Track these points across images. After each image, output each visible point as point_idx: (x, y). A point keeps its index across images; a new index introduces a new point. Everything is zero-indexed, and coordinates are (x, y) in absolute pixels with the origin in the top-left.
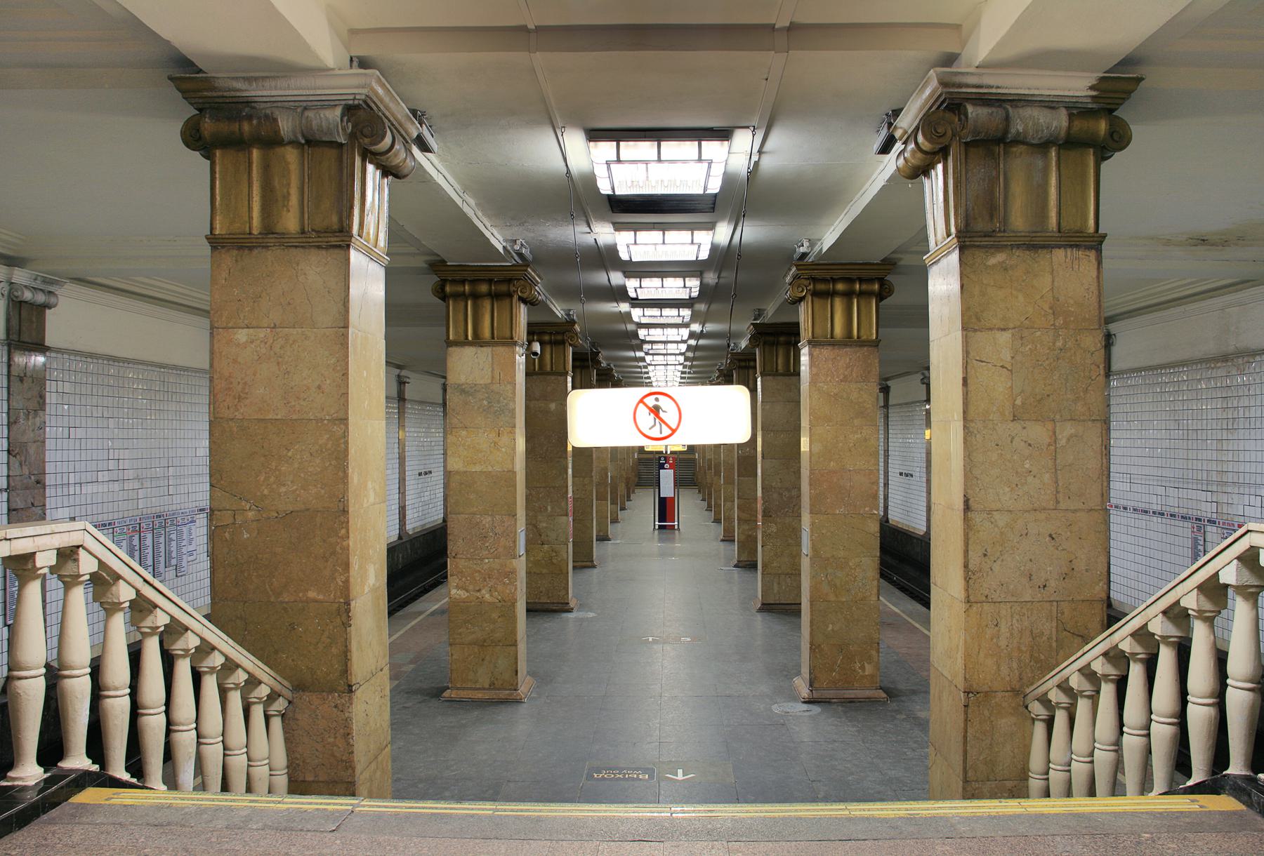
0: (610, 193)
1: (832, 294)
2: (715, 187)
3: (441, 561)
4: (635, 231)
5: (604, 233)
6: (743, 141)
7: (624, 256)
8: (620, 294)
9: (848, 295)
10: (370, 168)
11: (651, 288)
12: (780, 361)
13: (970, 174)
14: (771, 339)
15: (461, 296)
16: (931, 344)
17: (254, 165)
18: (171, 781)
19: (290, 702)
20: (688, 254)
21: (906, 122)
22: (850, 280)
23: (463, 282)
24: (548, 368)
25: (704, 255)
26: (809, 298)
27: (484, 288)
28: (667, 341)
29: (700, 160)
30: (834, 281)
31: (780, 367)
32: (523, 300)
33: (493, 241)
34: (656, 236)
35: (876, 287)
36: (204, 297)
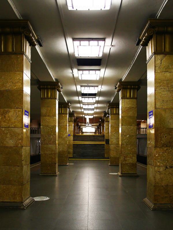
0: (81, 79)
2: (98, 79)
5: (80, 98)
6: (108, 41)
7: (83, 102)
9: (130, 89)
10: (58, 92)
11: (85, 100)
12: (115, 110)
14: (112, 106)
15: (44, 89)
19: (116, 152)
24: (63, 112)
25: (95, 102)
26: (154, 36)
27: (49, 87)
28: (88, 121)
29: (98, 45)
31: (115, 113)
32: (68, 108)
33: (65, 99)
34: (87, 99)
35: (137, 87)
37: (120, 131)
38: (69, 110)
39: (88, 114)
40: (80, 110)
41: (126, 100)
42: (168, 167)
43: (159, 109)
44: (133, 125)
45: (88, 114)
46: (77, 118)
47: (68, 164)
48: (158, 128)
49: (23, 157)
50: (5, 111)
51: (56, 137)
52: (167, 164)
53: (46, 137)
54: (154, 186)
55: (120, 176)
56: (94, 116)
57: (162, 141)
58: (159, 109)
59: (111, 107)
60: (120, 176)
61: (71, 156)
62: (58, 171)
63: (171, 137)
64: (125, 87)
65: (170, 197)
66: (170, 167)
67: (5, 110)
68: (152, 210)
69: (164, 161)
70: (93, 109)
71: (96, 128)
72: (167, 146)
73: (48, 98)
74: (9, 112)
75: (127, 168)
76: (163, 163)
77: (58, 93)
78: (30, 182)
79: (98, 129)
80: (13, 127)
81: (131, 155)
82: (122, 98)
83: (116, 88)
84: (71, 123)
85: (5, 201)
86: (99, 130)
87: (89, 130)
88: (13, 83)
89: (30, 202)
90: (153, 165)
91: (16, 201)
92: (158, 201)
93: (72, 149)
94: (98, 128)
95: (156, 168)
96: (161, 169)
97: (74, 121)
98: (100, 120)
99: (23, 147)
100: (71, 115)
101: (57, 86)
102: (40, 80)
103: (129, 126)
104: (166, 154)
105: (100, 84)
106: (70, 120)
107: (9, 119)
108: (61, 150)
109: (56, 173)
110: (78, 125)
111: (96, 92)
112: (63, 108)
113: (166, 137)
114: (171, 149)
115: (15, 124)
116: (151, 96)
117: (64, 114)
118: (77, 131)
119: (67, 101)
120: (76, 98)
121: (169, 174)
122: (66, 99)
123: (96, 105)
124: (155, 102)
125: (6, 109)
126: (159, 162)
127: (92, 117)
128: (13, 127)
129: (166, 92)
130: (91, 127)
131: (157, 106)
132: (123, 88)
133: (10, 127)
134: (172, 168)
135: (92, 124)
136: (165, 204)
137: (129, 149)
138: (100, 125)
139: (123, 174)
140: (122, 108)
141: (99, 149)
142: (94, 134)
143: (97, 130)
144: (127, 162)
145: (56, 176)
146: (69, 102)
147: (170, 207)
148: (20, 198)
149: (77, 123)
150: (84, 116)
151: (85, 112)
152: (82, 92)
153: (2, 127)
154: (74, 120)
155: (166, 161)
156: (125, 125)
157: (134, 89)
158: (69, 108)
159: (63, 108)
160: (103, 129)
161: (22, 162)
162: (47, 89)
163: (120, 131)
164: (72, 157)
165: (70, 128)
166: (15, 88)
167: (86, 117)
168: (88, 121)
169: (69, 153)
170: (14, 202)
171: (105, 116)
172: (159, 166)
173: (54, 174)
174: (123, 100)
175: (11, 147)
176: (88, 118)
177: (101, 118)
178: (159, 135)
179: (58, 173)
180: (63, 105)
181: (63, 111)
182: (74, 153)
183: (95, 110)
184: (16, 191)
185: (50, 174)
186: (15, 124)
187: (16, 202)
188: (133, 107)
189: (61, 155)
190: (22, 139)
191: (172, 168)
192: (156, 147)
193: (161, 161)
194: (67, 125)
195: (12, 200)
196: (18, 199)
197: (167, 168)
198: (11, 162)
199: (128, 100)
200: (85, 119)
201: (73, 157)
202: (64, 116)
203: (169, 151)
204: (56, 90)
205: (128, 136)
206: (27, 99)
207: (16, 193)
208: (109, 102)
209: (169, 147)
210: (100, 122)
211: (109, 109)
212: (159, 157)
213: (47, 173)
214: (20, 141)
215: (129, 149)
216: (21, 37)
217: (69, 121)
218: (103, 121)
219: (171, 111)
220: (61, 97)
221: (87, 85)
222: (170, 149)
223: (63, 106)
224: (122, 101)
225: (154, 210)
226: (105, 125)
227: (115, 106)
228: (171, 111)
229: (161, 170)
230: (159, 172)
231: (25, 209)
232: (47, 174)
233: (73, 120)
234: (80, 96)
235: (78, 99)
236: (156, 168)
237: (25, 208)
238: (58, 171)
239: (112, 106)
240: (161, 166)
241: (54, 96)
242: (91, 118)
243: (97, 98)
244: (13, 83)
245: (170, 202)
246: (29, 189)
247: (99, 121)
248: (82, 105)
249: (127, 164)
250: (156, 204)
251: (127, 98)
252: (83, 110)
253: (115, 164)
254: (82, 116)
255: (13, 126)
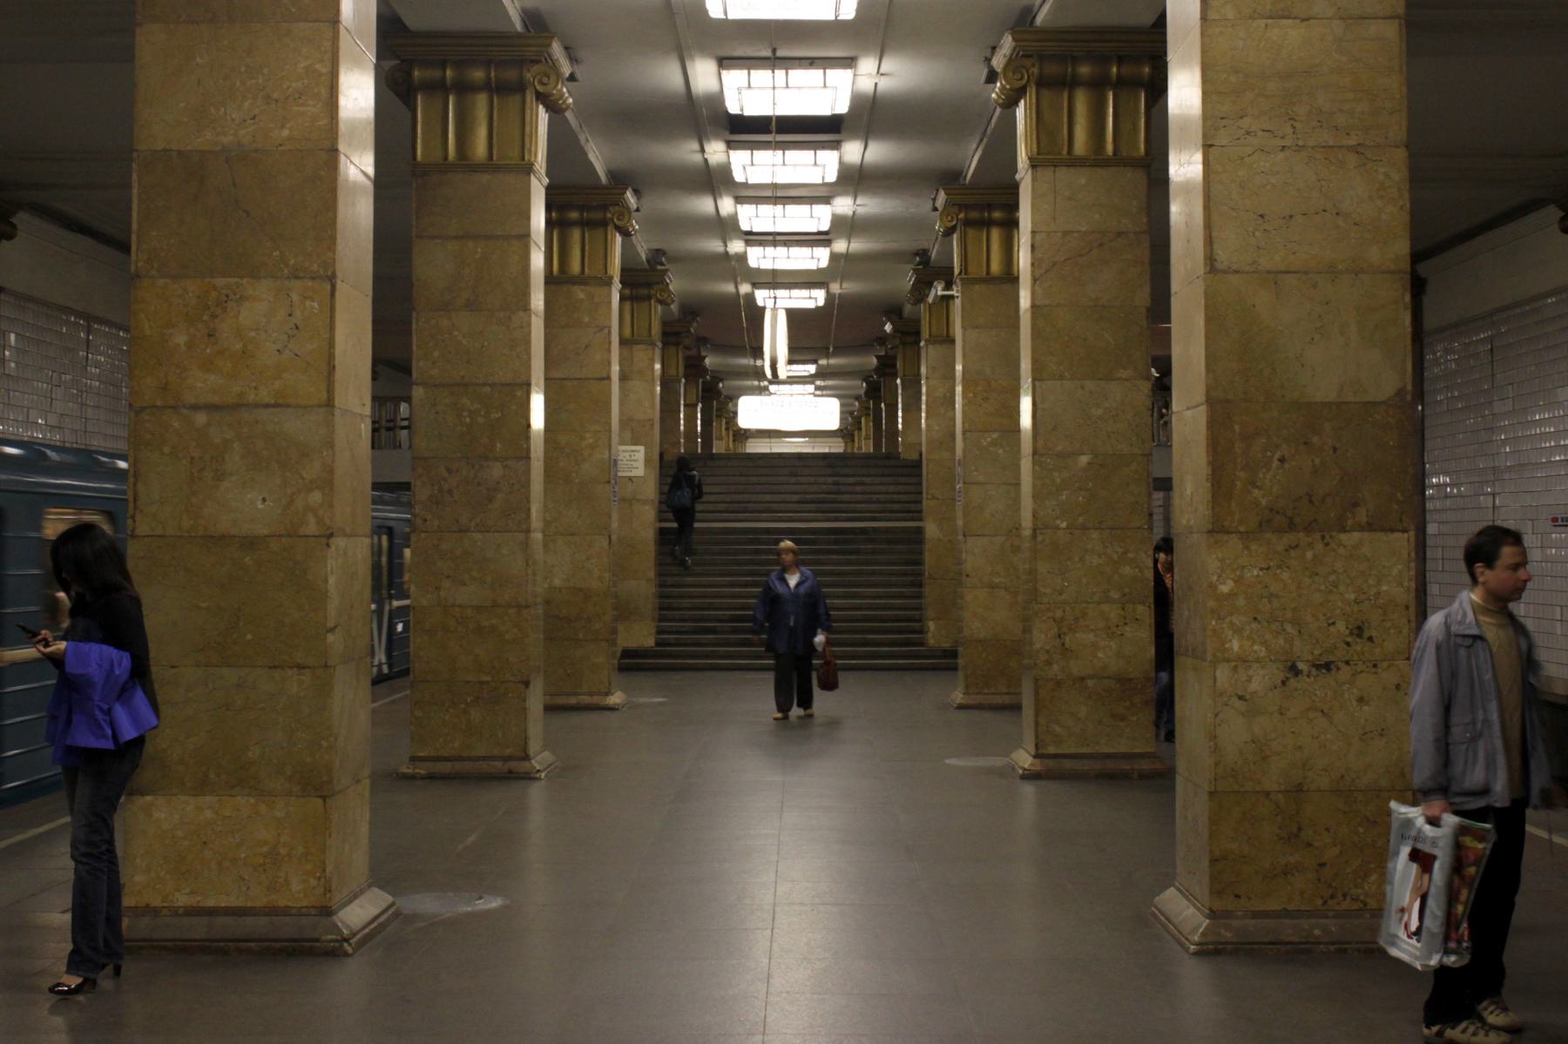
0: (722, 16)
1: (1071, 84)
3: (1395, 825)
4: (815, 150)
5: (716, 151)
6: (867, 65)
7: (739, 176)
8: (727, 227)
9: (1098, 85)
10: (541, 109)
11: (754, 165)
13: (355, 929)
14: (974, 215)
15: (437, 88)
16: (1173, 299)
17: (419, 141)
18: (124, 492)
20: (812, 176)
21: (998, 62)
22: (1103, 60)
23: (443, 65)
25: (832, 177)
26: (1031, 92)
28: (776, 337)
30: (1075, 60)
32: (542, 98)
33: (592, 157)
36: (33, 609)
37: (1026, 420)
38: (628, 249)
39: (776, 280)
40: (715, 246)
41: (1063, 173)
42: (1301, 666)
43: (1236, 272)
44: (1123, 374)
45: (776, 280)
46: (692, 310)
47: (616, 698)
48: (1227, 401)
49: (333, 605)
50: (214, 294)
51: (528, 472)
52: (1297, 642)
53: (449, 470)
54: (1211, 794)
55: (1030, 776)
56: (835, 288)
57: (1256, 492)
58: (1236, 272)
59: (968, 223)
60: (1030, 776)
61: (642, 635)
62: (545, 747)
63: (1317, 461)
64: (1052, 69)
65: (1322, 865)
66: (1318, 667)
67: (215, 288)
68: (1196, 954)
69: (1275, 626)
70: (819, 233)
71: (857, 398)
72: (1292, 526)
73: (465, 163)
74: (243, 299)
75: (1083, 711)
76: (1268, 636)
77: (543, 117)
78: (367, 782)
79: (871, 401)
80: (267, 406)
81: (1113, 612)
82: (1034, 164)
83: (992, 77)
84: (640, 354)
85: (211, 903)
86: (878, 411)
87: (791, 409)
88: (268, 99)
89: (376, 918)
90: (1204, 652)
91: (282, 903)
92: (1237, 896)
93: (652, 574)
94: (874, 392)
95: (1223, 674)
96: (1259, 681)
97: (665, 334)
98: (888, 328)
99: (331, 535)
100: (642, 281)
101: (536, 68)
102: (407, 23)
103: (1090, 385)
104: (1285, 575)
105: (866, 51)
106: (627, 332)
107: (238, 346)
108: (557, 582)
109: (527, 758)
110: (694, 367)
111: (842, 108)
112: (576, 234)
113: (1282, 460)
114: (1319, 546)
115: (277, 384)
116: (1187, 186)
117: (581, 280)
118: (691, 420)
119: (612, 174)
120: (686, 152)
121: (1311, 715)
122: (598, 157)
123: (844, 205)
124: (1208, 226)
125: (220, 282)
126: (1238, 631)
127: (813, 299)
128: (267, 406)
129: (1281, 156)
130: (811, 388)
131: (1222, 256)
132: (1041, 83)
133: (248, 405)
134: (1329, 670)
135: (823, 362)
136: (1286, 914)
137: (1096, 561)
138: (887, 367)
139: (1051, 763)
140: (1038, 237)
141: (874, 573)
142: (836, 447)
143: (865, 410)
144: (1076, 668)
145: (529, 777)
146: (621, 179)
147: (1317, 932)
148: (313, 882)
149: (694, 352)
150: (745, 288)
151: (758, 258)
152: (733, 108)
153: (195, 407)
154: (664, 323)
155: (1289, 628)
156: (1062, 377)
157: (1121, 84)
158: (626, 234)
159: (481, 101)
160: (912, 407)
161: (331, 638)
162: (464, 89)
163: (1026, 420)
164: (650, 642)
165: (632, 385)
166: (286, 133)
167: (762, 297)
168: (776, 337)
169: (624, 612)
170: (273, 911)
171: (922, 285)
172: (1243, 661)
173: (513, 765)
174: (1047, 174)
175: (250, 543)
176: (777, 305)
177: (893, 311)
178: (1239, 447)
179: (547, 756)
180: (583, 205)
181: (482, 133)
182: (666, 607)
183: (840, 246)
184: (283, 839)
185: (484, 766)
186: (277, 384)
187: (284, 912)
188: (1119, 234)
189: (565, 622)
190: (327, 483)
191: (1329, 670)
192: (1217, 529)
193: (1255, 625)
194: (608, 378)
195: (259, 898)
196: (297, 890)
197: (1294, 670)
198: (249, 637)
199: (1081, 177)
200: (757, 314)
201: (658, 644)
202: (581, 296)
203: (1309, 555)
204: (530, 97)
205: (1084, 460)
206: (358, 213)
207: (283, 851)
208: (949, 178)
209: (1308, 529)
210: (882, 339)
211: (949, 232)
212: (1241, 602)
213: (462, 759)
214: (316, 497)
215: (1096, 561)
216: (524, 102)
217: (623, 342)
218: (909, 334)
219: (1315, 286)
220: (563, 146)
221: (768, 53)
222: (1311, 545)
223: (574, 215)
224: (1034, 180)
225: (1211, 951)
226: (923, 370)
227: (997, 215)
228: (1315, 286)
229: (1254, 686)
230: (1241, 698)
231: (346, 955)
232: (458, 766)
233: (656, 329)
234: (717, 137)
235: (698, 158)
236: (1218, 673)
237: (349, 950)
238: (545, 747)
239: (974, 215)
240: (1258, 661)
241: (516, 154)
242: (810, 305)
243: (853, 151)
244: (268, 99)
245: (1320, 902)
246: (364, 829)
247: (868, 337)
248: (727, 205)
249: (1083, 679)
250: (1227, 914)
251: (1074, 162)
252: (736, 246)
253: (999, 686)
254: (730, 288)
255: (265, 395)
